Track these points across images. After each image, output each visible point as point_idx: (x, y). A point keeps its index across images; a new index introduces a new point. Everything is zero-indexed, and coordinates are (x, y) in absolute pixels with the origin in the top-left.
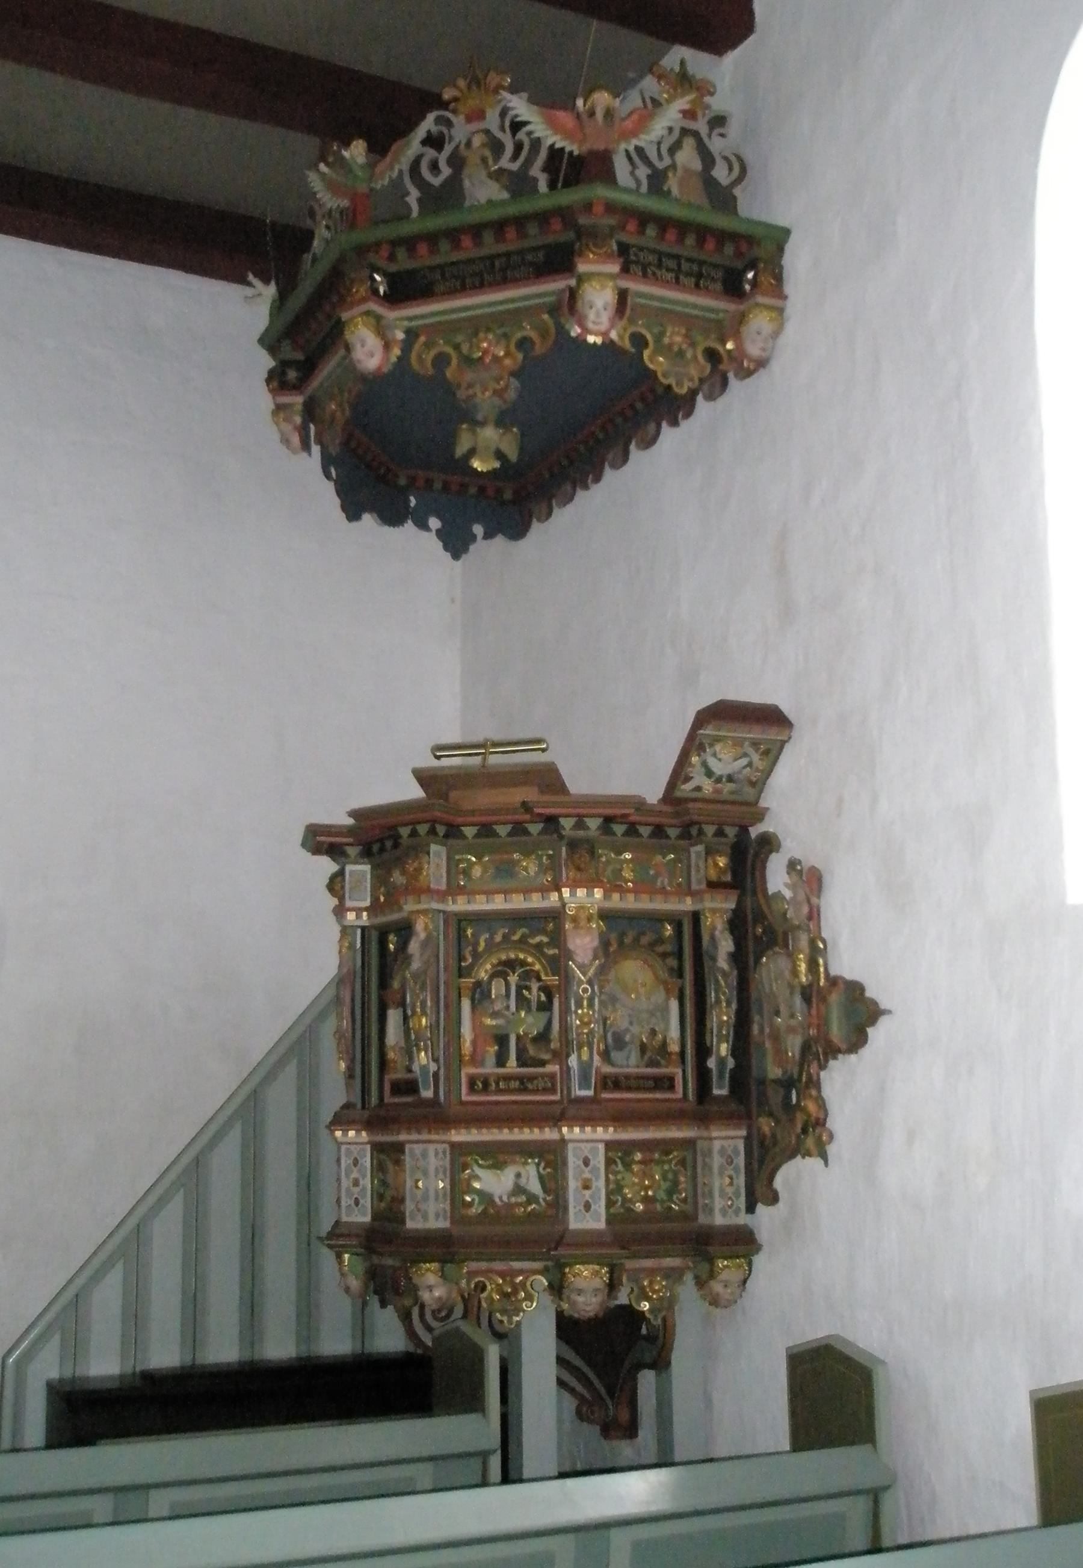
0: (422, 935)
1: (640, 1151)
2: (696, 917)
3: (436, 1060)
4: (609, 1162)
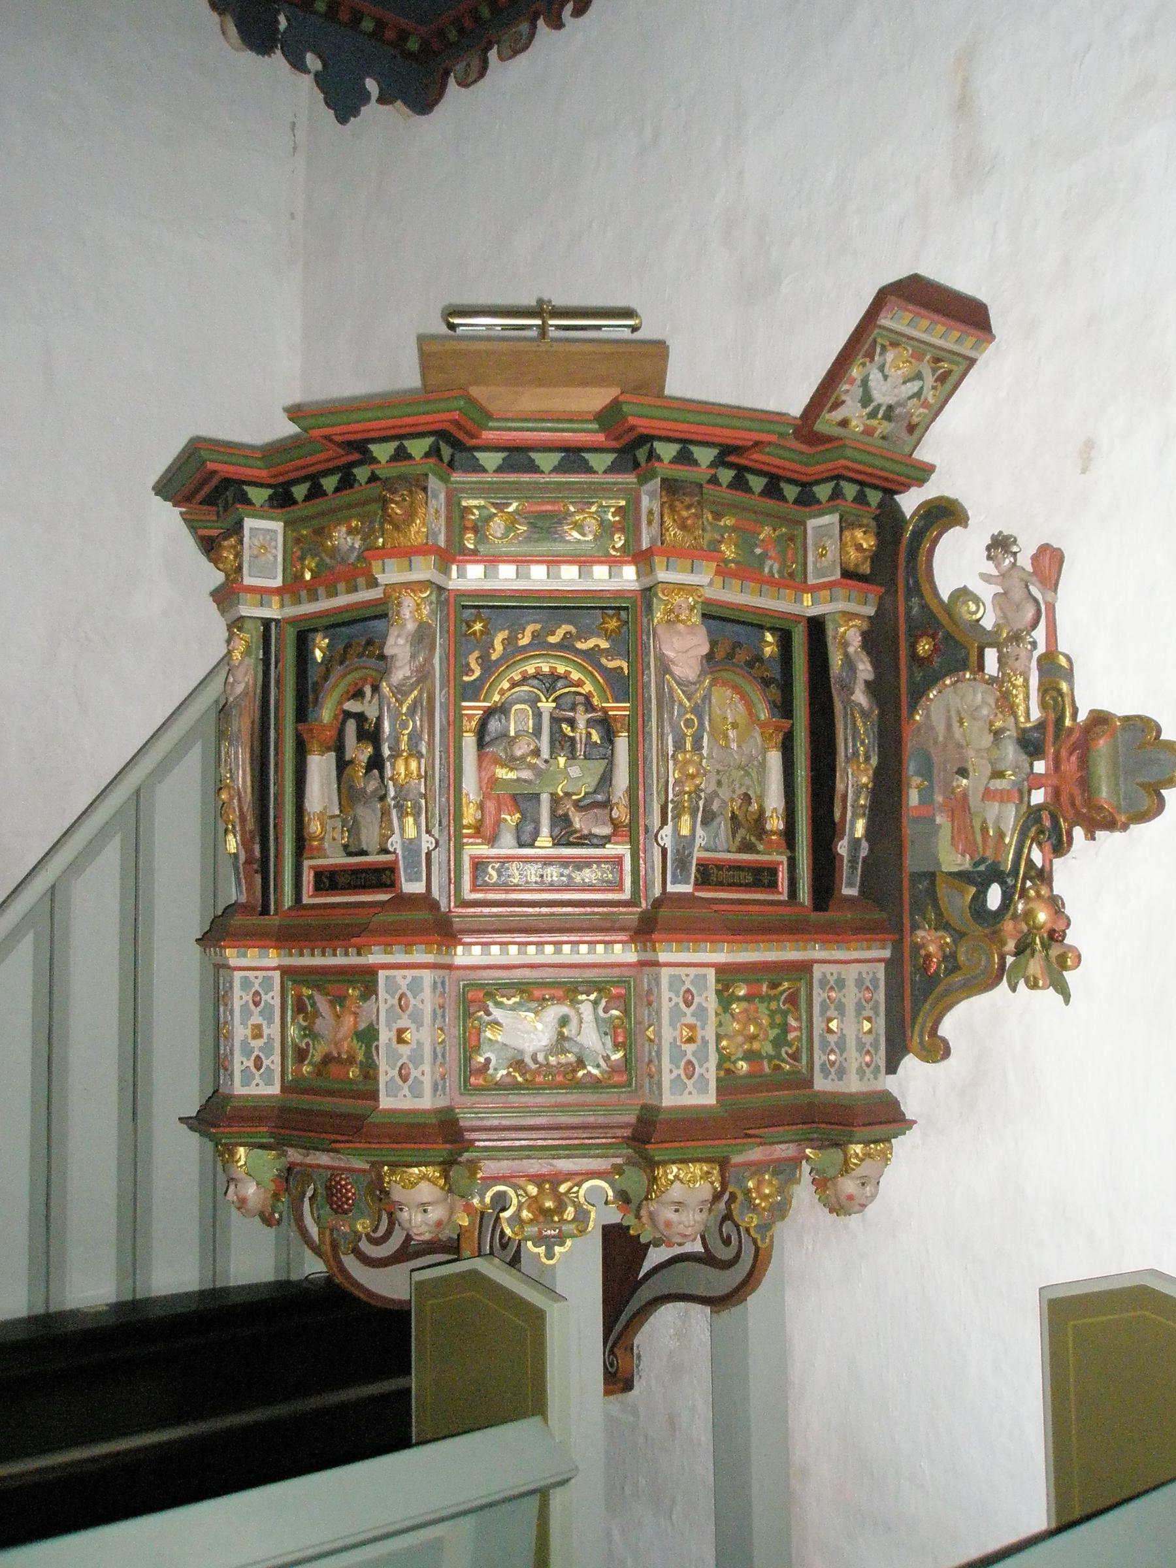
0: (411, 626)
2: (816, 626)
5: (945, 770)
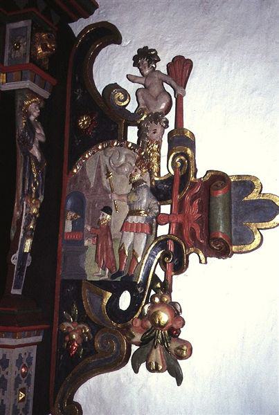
5: (94, 207)
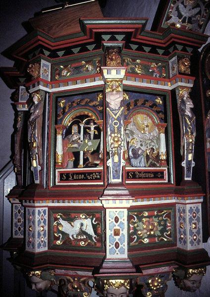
1: (147, 211)
3: (42, 165)
4: (130, 218)
